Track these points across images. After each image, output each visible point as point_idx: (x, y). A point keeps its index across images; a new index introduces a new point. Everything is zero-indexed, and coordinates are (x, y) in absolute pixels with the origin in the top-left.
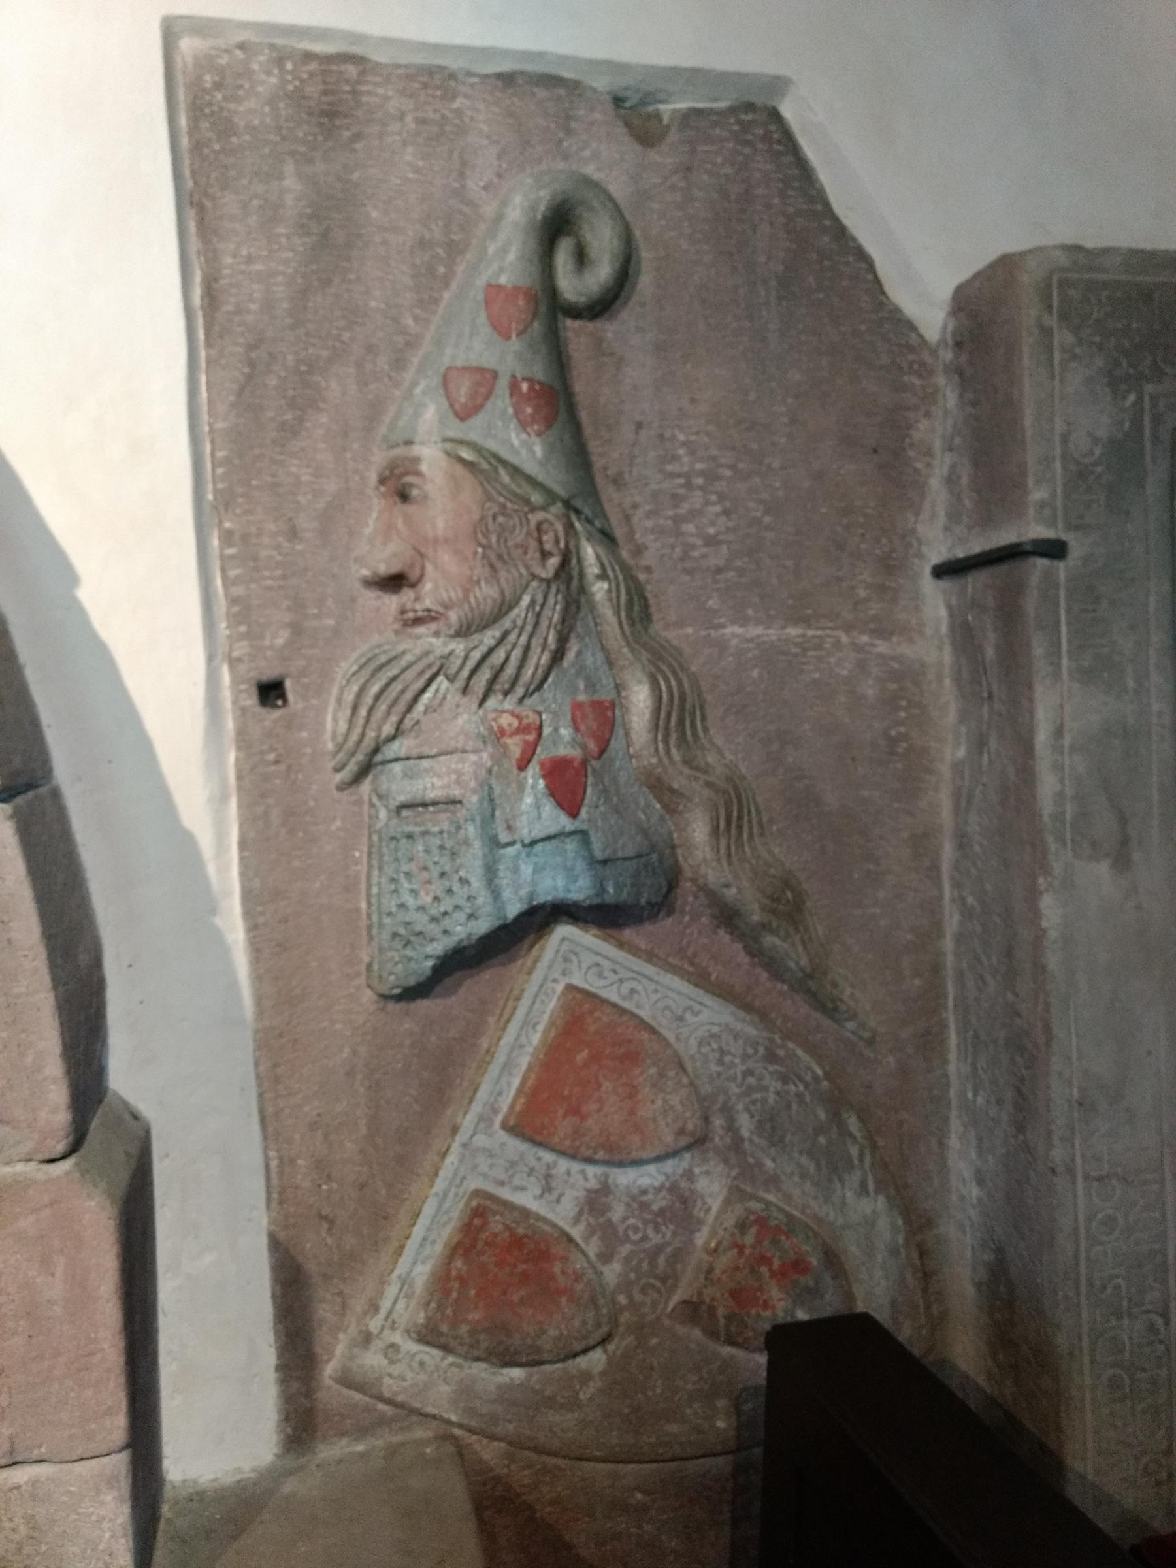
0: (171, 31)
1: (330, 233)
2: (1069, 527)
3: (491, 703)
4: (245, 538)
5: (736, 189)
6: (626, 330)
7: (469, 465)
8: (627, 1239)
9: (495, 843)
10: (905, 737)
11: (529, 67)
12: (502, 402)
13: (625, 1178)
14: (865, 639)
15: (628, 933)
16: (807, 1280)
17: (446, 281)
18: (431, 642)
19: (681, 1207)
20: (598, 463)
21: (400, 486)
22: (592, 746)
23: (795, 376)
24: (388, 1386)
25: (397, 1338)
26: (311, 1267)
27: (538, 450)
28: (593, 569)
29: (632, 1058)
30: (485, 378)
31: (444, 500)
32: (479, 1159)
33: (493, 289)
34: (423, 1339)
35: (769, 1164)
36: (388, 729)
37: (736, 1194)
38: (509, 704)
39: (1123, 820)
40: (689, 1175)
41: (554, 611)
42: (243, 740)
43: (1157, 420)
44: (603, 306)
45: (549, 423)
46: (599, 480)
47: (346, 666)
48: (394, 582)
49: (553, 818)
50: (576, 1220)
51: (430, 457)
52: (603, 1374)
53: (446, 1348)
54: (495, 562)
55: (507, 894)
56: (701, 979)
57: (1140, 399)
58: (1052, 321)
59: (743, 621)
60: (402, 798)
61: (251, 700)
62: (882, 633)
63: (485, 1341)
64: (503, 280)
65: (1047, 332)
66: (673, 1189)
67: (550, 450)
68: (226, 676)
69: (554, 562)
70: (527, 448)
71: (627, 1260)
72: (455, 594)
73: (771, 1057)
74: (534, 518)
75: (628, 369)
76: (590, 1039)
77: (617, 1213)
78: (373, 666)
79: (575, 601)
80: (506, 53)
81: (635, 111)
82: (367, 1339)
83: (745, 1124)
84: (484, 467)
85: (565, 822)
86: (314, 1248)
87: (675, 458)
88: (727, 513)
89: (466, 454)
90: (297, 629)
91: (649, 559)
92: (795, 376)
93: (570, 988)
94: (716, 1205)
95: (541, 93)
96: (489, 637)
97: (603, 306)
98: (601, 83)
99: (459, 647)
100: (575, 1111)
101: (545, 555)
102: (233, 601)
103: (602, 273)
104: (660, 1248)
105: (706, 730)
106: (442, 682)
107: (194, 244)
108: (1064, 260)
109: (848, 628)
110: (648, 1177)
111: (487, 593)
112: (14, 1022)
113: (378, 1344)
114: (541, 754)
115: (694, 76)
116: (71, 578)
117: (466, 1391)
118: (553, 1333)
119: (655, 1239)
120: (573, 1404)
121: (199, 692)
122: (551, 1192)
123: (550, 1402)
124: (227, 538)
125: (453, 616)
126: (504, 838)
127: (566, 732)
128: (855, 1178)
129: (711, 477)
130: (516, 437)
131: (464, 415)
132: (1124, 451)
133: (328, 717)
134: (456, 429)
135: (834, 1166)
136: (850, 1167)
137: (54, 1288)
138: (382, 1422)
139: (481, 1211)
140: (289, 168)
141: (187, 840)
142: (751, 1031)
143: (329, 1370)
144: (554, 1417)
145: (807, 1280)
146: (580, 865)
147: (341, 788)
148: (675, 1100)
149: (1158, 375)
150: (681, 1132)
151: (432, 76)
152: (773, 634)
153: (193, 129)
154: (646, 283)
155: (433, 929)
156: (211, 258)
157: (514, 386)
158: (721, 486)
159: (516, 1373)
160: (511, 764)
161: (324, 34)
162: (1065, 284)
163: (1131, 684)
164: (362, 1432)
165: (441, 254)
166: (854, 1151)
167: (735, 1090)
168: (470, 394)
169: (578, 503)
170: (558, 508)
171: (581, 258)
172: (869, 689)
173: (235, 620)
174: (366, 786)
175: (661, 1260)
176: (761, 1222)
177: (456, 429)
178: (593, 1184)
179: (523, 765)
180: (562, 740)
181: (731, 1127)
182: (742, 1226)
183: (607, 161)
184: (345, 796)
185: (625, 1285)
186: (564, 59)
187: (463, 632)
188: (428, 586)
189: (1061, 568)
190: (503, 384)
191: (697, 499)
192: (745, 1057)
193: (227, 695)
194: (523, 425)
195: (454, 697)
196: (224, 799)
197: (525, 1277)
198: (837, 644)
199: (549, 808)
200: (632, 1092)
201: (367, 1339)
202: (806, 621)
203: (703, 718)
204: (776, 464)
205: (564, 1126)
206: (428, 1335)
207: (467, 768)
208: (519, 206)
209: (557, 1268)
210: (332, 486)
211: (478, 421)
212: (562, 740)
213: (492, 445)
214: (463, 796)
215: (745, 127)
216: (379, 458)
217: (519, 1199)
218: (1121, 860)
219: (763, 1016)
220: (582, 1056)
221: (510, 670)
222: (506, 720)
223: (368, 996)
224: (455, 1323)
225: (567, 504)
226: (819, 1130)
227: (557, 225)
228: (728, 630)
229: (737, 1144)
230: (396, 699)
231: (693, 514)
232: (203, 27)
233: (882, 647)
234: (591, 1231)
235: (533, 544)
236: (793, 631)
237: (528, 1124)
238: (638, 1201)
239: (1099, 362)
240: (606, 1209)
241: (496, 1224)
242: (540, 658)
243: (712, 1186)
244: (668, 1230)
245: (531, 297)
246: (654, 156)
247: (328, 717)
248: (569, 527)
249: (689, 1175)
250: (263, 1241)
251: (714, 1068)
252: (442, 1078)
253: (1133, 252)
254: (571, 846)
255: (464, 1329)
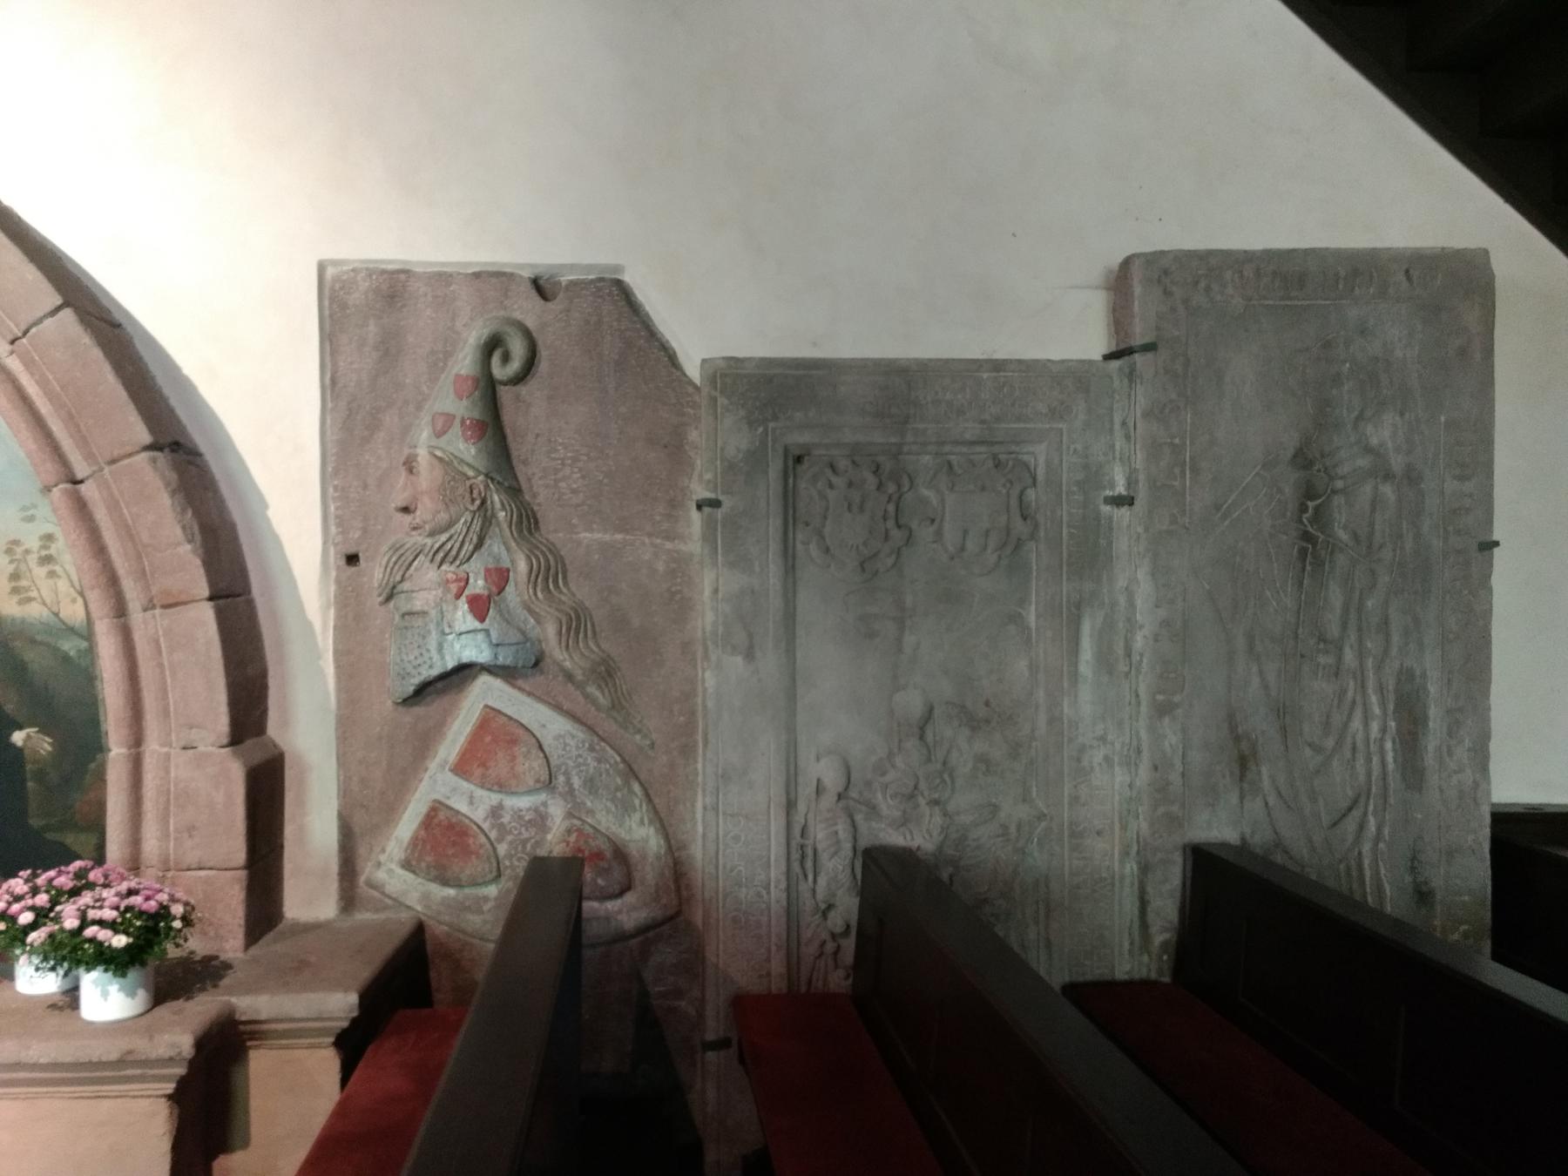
0: (322, 268)
1: (389, 350)
2: (723, 493)
3: (444, 567)
4: (343, 489)
5: (594, 319)
6: (532, 390)
7: (440, 459)
8: (510, 832)
9: (443, 633)
10: (680, 592)
11: (490, 269)
12: (456, 428)
13: (512, 802)
14: (659, 541)
15: (520, 682)
16: (604, 864)
17: (443, 369)
18: (419, 539)
19: (540, 820)
20: (514, 453)
21: (410, 465)
22: (494, 590)
23: (623, 410)
24: (389, 889)
25: (393, 866)
26: (357, 830)
27: (473, 451)
28: (498, 505)
29: (514, 742)
30: (450, 418)
31: (428, 475)
32: (439, 784)
33: (458, 376)
34: (403, 867)
35: (589, 804)
36: (398, 578)
37: (569, 815)
38: (452, 568)
39: (750, 636)
40: (545, 804)
41: (477, 526)
42: (338, 581)
43: (774, 441)
44: (520, 378)
45: (480, 438)
46: (515, 462)
47: (385, 548)
48: (405, 510)
49: (472, 623)
50: (485, 819)
51: (422, 453)
52: (496, 899)
53: (414, 872)
54: (448, 502)
55: (448, 658)
56: (558, 708)
57: (766, 430)
58: (717, 394)
59: (591, 530)
60: (404, 610)
61: (343, 562)
62: (668, 538)
63: (434, 873)
64: (463, 372)
65: (715, 400)
66: (536, 810)
67: (479, 451)
68: (332, 551)
69: (478, 502)
70: (467, 450)
71: (511, 843)
72: (428, 517)
73: (592, 749)
74: (468, 483)
75: (529, 413)
76: (495, 734)
77: (506, 819)
78: (395, 548)
79: (488, 520)
80: (477, 264)
81: (541, 287)
82: (379, 864)
83: (576, 782)
84: (446, 463)
85: (477, 625)
86: (359, 820)
87: (556, 451)
88: (583, 477)
89: (439, 453)
90: (365, 531)
91: (540, 499)
92: (623, 410)
93: (486, 706)
94: (558, 820)
95: (494, 280)
96: (443, 538)
97: (520, 378)
98: (527, 274)
99: (429, 541)
100: (483, 765)
101: (473, 500)
102: (337, 517)
103: (515, 366)
104: (527, 840)
105: (566, 583)
106: (421, 557)
107: (328, 359)
108: (722, 364)
109: (650, 535)
110: (524, 802)
111: (443, 517)
112: (363, 806)
113: (384, 868)
114: (467, 592)
115: (572, 267)
116: (266, 506)
117: (426, 897)
118: (468, 872)
119: (526, 835)
120: (480, 912)
121: (318, 558)
122: (472, 803)
123: (468, 909)
124: (336, 488)
125: (427, 527)
126: (447, 630)
127: (481, 582)
128: (637, 816)
129: (575, 460)
130: (462, 446)
131: (439, 435)
132: (756, 459)
133: (375, 573)
134: (434, 442)
135: (626, 808)
136: (635, 810)
137: (219, 797)
138: (386, 908)
139: (436, 808)
140: (372, 322)
141: (308, 625)
142: (581, 735)
143: (362, 879)
144: (470, 917)
145: (604, 864)
146: (484, 646)
147: (382, 604)
148: (535, 764)
149: (775, 418)
150: (538, 781)
151: (442, 278)
152: (607, 537)
153: (330, 308)
154: (543, 366)
155: (414, 672)
156: (335, 364)
157: (463, 422)
158: (580, 464)
159: (451, 892)
160: (450, 596)
161: (390, 262)
162: (724, 375)
163: (757, 569)
164: (377, 911)
165: (440, 359)
166: (637, 802)
167: (571, 763)
168: (442, 426)
169: (494, 475)
170: (481, 478)
171: (506, 358)
172: (661, 567)
173: (338, 525)
174: (392, 604)
175: (529, 846)
176: (579, 831)
177: (434, 442)
178: (494, 803)
179: (458, 596)
180: (478, 585)
181: (568, 782)
182: (569, 831)
183: (528, 310)
184: (383, 609)
185: (510, 856)
186: (505, 264)
187: (432, 534)
188: (418, 513)
189: (719, 513)
190: (457, 422)
191: (567, 471)
192: (578, 748)
193: (332, 559)
194: (466, 441)
195: (427, 564)
196: (328, 608)
197: (454, 844)
198: (643, 544)
199: (470, 617)
200: (514, 758)
201: (379, 864)
202: (626, 532)
203: (565, 578)
204: (612, 453)
205: (478, 772)
206: (407, 865)
207: (431, 597)
208: (473, 337)
209: (471, 841)
210: (384, 465)
211: (445, 438)
212: (478, 585)
213: (451, 449)
214: (17, 568)
215: (599, 289)
216: (406, 451)
217: (457, 806)
218: (749, 655)
219: (591, 729)
220: (488, 739)
221: (454, 553)
222: (450, 576)
223: (389, 703)
224: (419, 860)
225: (487, 475)
226: (617, 789)
227: (493, 345)
228: (582, 535)
229: (571, 791)
230: (404, 562)
231: (564, 479)
232: (335, 263)
233: (669, 545)
234: (493, 826)
235: (467, 495)
236: (619, 537)
237: (461, 768)
238: (518, 815)
239: (742, 413)
240: (501, 816)
241: (442, 815)
242: (468, 547)
243: (557, 810)
244: (533, 831)
245: (476, 381)
246: (549, 305)
247: (375, 573)
248: (487, 487)
249: (545, 804)
250: (335, 813)
251: (561, 752)
252: (424, 744)
253: (763, 359)
254: (480, 636)
255: (423, 865)
